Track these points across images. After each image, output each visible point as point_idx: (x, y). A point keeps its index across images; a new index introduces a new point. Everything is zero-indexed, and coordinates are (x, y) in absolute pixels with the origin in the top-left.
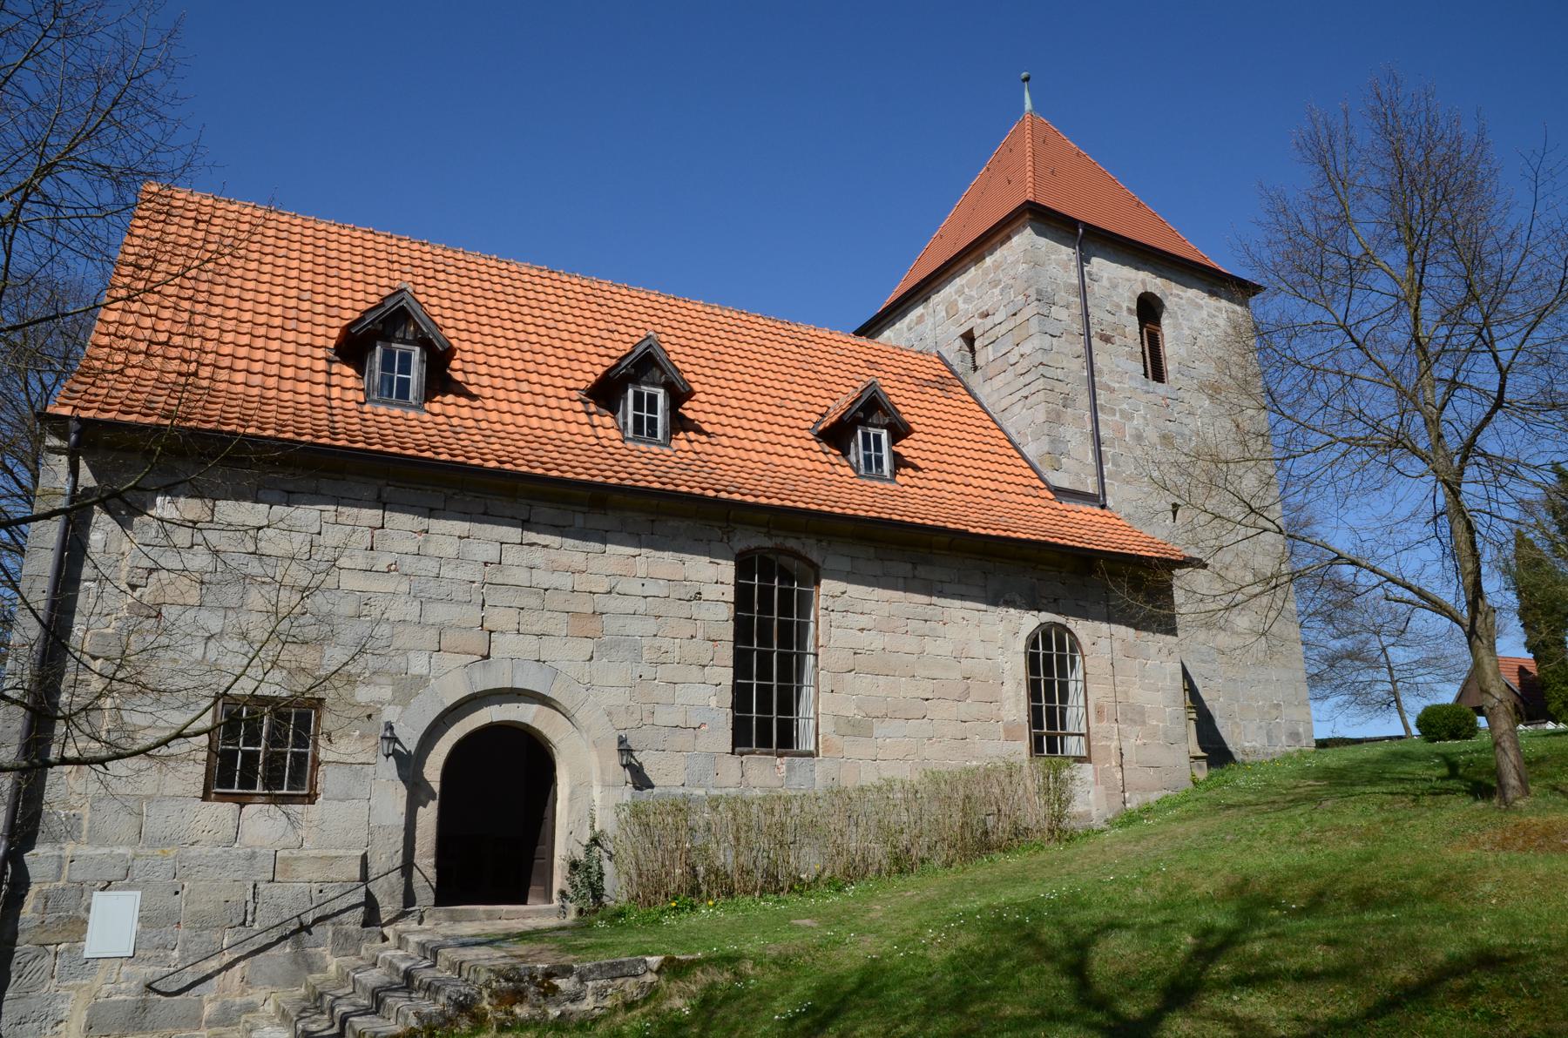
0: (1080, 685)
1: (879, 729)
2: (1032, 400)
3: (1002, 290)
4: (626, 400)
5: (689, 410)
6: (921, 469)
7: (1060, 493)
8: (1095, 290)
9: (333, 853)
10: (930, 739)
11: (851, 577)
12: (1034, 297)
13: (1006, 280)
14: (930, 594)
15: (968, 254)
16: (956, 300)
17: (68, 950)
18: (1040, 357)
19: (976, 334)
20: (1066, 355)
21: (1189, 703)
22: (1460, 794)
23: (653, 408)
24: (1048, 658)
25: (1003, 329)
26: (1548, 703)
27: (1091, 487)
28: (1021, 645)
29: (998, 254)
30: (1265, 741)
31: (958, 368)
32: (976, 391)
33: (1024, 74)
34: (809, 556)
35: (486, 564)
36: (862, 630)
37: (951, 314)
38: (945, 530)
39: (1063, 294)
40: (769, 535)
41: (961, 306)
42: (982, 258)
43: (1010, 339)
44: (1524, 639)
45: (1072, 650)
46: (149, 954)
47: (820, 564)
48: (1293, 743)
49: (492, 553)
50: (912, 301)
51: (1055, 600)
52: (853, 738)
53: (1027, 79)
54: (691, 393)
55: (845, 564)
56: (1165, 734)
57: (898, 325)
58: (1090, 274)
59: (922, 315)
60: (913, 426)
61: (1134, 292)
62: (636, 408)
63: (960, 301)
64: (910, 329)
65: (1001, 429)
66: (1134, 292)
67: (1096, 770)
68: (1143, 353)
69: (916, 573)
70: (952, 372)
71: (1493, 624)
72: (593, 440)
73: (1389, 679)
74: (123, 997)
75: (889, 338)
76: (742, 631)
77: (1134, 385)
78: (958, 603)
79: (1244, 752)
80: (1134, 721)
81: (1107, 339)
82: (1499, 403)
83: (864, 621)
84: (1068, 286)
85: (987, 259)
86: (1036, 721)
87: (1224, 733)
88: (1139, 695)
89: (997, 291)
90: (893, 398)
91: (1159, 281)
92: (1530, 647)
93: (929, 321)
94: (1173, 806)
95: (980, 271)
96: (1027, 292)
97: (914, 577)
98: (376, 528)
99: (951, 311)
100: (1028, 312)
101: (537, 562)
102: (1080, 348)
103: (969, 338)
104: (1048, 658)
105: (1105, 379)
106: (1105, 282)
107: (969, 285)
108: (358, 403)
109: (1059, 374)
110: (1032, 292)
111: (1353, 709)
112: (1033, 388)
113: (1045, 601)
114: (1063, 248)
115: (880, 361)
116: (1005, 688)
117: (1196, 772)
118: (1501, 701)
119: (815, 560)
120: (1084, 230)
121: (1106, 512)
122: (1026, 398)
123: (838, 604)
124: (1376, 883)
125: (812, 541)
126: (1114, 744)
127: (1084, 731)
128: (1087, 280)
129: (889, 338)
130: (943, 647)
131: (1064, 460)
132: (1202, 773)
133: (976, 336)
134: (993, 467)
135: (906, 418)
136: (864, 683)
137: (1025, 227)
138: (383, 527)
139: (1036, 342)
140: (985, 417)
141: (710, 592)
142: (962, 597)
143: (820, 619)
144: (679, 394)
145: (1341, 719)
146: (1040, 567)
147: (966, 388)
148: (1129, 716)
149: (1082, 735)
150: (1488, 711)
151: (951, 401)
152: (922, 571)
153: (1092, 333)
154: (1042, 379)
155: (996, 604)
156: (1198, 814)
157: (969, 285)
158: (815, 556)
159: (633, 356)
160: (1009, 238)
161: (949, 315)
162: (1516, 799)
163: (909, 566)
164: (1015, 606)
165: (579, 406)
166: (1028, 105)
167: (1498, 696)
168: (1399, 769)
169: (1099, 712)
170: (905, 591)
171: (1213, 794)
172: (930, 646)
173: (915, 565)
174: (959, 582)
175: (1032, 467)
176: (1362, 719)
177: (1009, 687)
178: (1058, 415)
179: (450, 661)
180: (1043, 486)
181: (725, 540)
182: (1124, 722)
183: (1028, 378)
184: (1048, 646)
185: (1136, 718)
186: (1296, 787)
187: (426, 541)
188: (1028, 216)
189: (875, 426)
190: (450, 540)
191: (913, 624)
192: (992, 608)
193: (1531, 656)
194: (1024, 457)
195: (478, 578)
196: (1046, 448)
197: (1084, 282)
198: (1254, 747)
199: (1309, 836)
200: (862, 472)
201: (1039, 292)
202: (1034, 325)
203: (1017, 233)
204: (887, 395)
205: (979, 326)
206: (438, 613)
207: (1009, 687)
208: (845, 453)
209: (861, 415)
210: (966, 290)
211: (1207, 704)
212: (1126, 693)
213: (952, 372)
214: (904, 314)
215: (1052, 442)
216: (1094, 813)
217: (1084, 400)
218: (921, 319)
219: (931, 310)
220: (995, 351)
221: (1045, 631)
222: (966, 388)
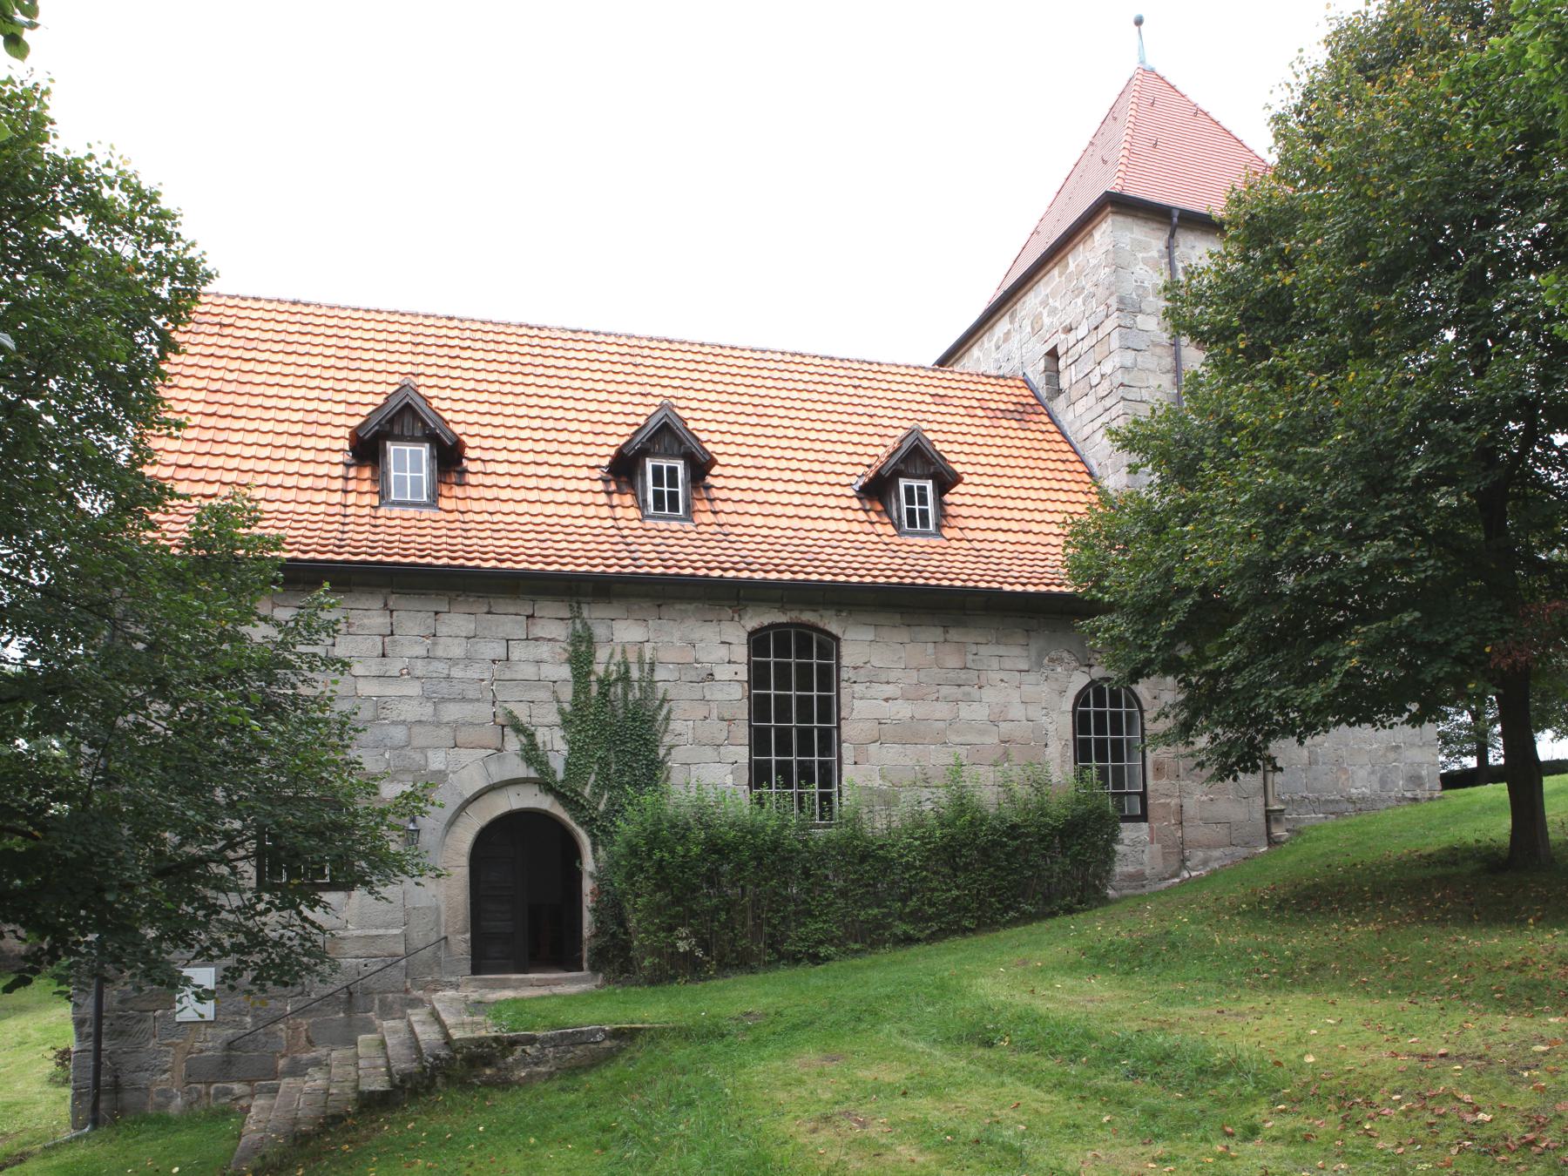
4: (644, 474)
9: (374, 932)
12: (1114, 307)
13: (1089, 288)
16: (1041, 313)
17: (163, 1016)
18: (1119, 377)
19: (1060, 351)
23: (673, 482)
25: (1085, 345)
28: (1068, 705)
30: (1376, 786)
31: (1043, 393)
35: (494, 661)
36: (886, 700)
39: (1151, 298)
40: (783, 610)
41: (1047, 320)
46: (229, 1018)
47: (840, 635)
49: (499, 650)
50: (998, 316)
54: (713, 462)
59: (1008, 333)
64: (998, 348)
67: (1151, 829)
70: (1036, 397)
72: (874, 538)
74: (211, 1053)
76: (759, 708)
83: (889, 690)
89: (1080, 301)
98: (384, 636)
100: (1109, 325)
101: (545, 656)
107: (1053, 294)
108: (373, 507)
110: (1113, 301)
115: (950, 393)
116: (1048, 750)
119: (834, 632)
130: (975, 712)
135: (958, 468)
138: (392, 634)
141: (723, 673)
144: (700, 466)
157: (1053, 294)
158: (834, 628)
159: (648, 429)
161: (1035, 332)
163: (939, 631)
165: (599, 486)
172: (966, 712)
174: (998, 643)
179: (465, 755)
181: (736, 618)
183: (1108, 402)
187: (435, 644)
190: (457, 641)
191: (945, 690)
195: (486, 675)
198: (1363, 793)
201: (1121, 300)
202: (1115, 342)
204: (931, 442)
205: (1062, 341)
206: (452, 712)
208: (887, 512)
210: (1051, 300)
213: (1036, 397)
218: (1007, 335)
222: (1049, 415)
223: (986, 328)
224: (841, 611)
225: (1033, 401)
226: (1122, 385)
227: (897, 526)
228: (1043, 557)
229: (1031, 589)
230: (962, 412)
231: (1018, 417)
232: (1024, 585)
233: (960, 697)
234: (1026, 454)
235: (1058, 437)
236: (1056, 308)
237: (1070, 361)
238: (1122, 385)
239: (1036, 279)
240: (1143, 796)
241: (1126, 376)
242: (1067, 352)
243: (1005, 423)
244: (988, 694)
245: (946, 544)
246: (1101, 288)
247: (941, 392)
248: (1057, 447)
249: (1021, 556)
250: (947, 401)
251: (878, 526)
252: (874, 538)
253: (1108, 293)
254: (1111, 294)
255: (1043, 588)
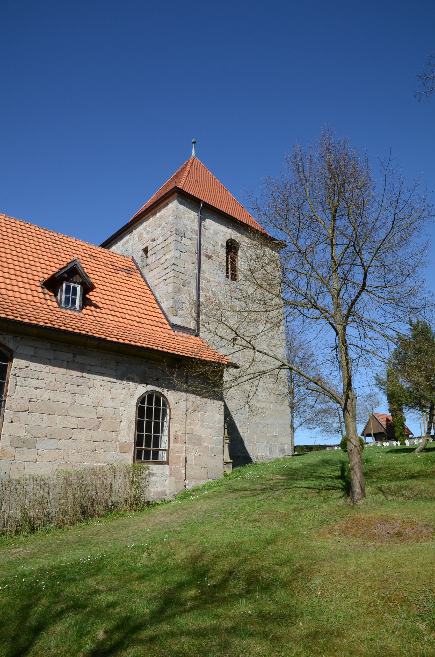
0: (168, 424)
1: (40, 444)
2: (168, 281)
3: (162, 229)
5: (92, 296)
6: (100, 308)
7: (174, 327)
8: (206, 234)
10: (72, 450)
11: (32, 359)
12: (174, 233)
13: (164, 224)
14: (83, 372)
15: (150, 211)
16: (143, 233)
18: (173, 261)
20: (187, 262)
21: (226, 435)
22: (338, 490)
23: (74, 293)
24: (150, 410)
26: (395, 433)
27: (192, 325)
28: (134, 402)
29: (162, 212)
32: (146, 276)
33: (193, 140)
34: (6, 344)
36: (36, 388)
37: (140, 239)
38: (92, 337)
39: (189, 233)
41: (145, 235)
42: (155, 214)
43: (162, 252)
44: (388, 408)
45: (164, 405)
47: (14, 350)
48: (281, 454)
51: (157, 379)
52: (22, 449)
53: (194, 143)
55: (31, 351)
56: (212, 451)
57: (118, 244)
58: (204, 226)
59: (128, 240)
60: (96, 285)
61: (225, 238)
62: (66, 293)
63: (144, 233)
64: (123, 246)
65: (153, 295)
66: (225, 238)
67: (171, 469)
68: (227, 266)
69: (76, 359)
71: (355, 405)
72: (45, 306)
73: (339, 421)
75: (114, 250)
77: (220, 280)
78: (99, 377)
79: (257, 458)
80: (195, 444)
81: (209, 257)
82: (363, 287)
83: (38, 383)
84: (192, 230)
85: (158, 214)
86: (139, 441)
87: (248, 448)
88: (199, 430)
89: (159, 229)
90: (86, 270)
91: (238, 235)
92: (391, 411)
93: (131, 242)
94: (210, 488)
95: (154, 220)
96: (172, 230)
97: (74, 361)
99: (140, 239)
102: (195, 259)
103: (146, 250)
104: (150, 410)
105: (206, 275)
106: (211, 231)
109: (183, 270)
110: (174, 230)
111: (325, 434)
112: (169, 275)
113: (151, 380)
114: (192, 212)
117: (226, 469)
118: (356, 446)
119: (11, 347)
120: (203, 205)
121: (197, 338)
122: (166, 280)
123: (23, 373)
124: (263, 568)
125: (11, 337)
126: (182, 455)
127: (167, 448)
128: (202, 228)
129: (114, 250)
130: (87, 401)
131: (180, 312)
132: (229, 471)
133: (149, 250)
134: (141, 311)
135: (93, 281)
136: (34, 418)
137: (174, 200)
139: (172, 254)
140: (147, 288)
142: (102, 374)
143: (10, 381)
145: (320, 437)
146: (150, 361)
147: (141, 274)
148: (193, 441)
149: (165, 450)
150: (349, 451)
151: (131, 279)
152: (79, 359)
153: (202, 253)
154: (173, 271)
155: (122, 379)
156: (218, 495)
157: (149, 226)
158: (11, 345)
160: (167, 204)
162: (358, 500)
163: (71, 356)
164: (133, 380)
165: (40, 289)
166: (193, 154)
167: (354, 443)
168: (321, 471)
169: (176, 439)
170: (67, 368)
171: (230, 482)
172: (79, 399)
173: (74, 355)
174: (101, 366)
175: (164, 314)
176: (328, 437)
177: (125, 424)
178: (179, 289)
180: (166, 322)
182: (190, 444)
184: (150, 403)
185: (197, 442)
186: (272, 479)
188: (176, 194)
189: (74, 283)
191: (69, 387)
192: (119, 381)
193: (390, 414)
194: (161, 308)
196: (171, 305)
197: (200, 229)
198: (263, 456)
199: (256, 516)
200: (63, 305)
201: (177, 230)
202: (172, 246)
203: (171, 202)
204: (83, 268)
205: (150, 245)
207: (125, 424)
208: (56, 295)
209: (66, 276)
210: (147, 228)
211: (241, 434)
212: (192, 429)
213: (137, 266)
214: (121, 239)
215: (174, 302)
216: (168, 491)
217: (193, 284)
219: (132, 237)
220: (155, 257)
221: (150, 395)
222: (141, 274)
223: (119, 237)
224: (16, 337)
225: (135, 268)
226: (174, 264)
227: (59, 303)
228: (130, 330)
229: (121, 341)
230: (102, 264)
231: (127, 272)
232: (118, 339)
233: (78, 392)
234: (128, 286)
235: (144, 284)
236: (149, 231)
237: (153, 253)
238: (174, 264)
239: (142, 219)
240: (168, 451)
241: (176, 261)
242: (151, 249)
243: (120, 272)
244: (93, 392)
245: (82, 316)
246: (169, 225)
247: (94, 255)
248: (143, 287)
249: (119, 328)
250: (96, 258)
251: (49, 302)
252: (45, 306)
253: (172, 227)
254: (173, 227)
255: (127, 342)
